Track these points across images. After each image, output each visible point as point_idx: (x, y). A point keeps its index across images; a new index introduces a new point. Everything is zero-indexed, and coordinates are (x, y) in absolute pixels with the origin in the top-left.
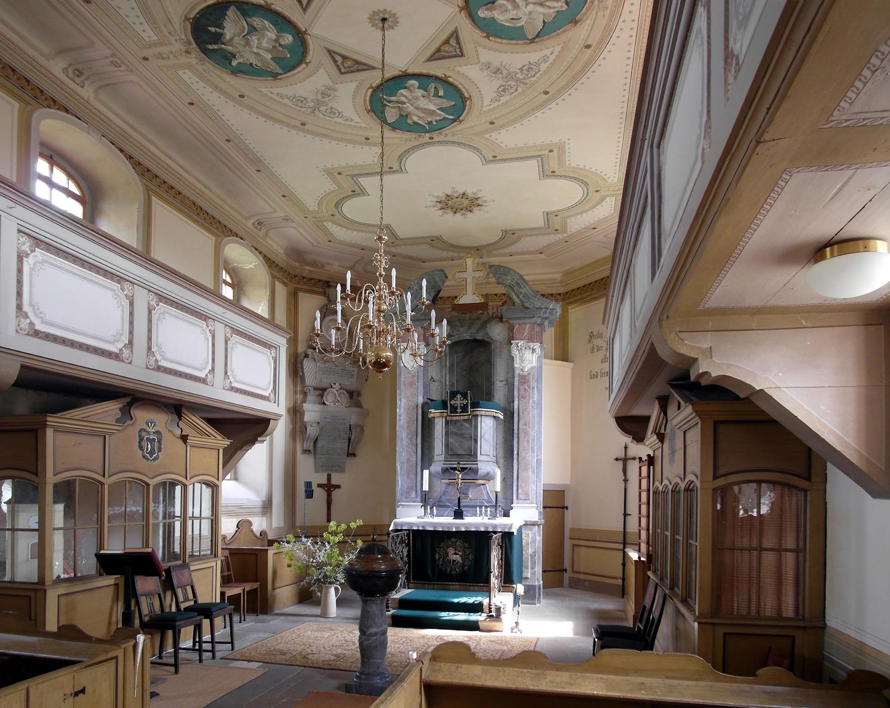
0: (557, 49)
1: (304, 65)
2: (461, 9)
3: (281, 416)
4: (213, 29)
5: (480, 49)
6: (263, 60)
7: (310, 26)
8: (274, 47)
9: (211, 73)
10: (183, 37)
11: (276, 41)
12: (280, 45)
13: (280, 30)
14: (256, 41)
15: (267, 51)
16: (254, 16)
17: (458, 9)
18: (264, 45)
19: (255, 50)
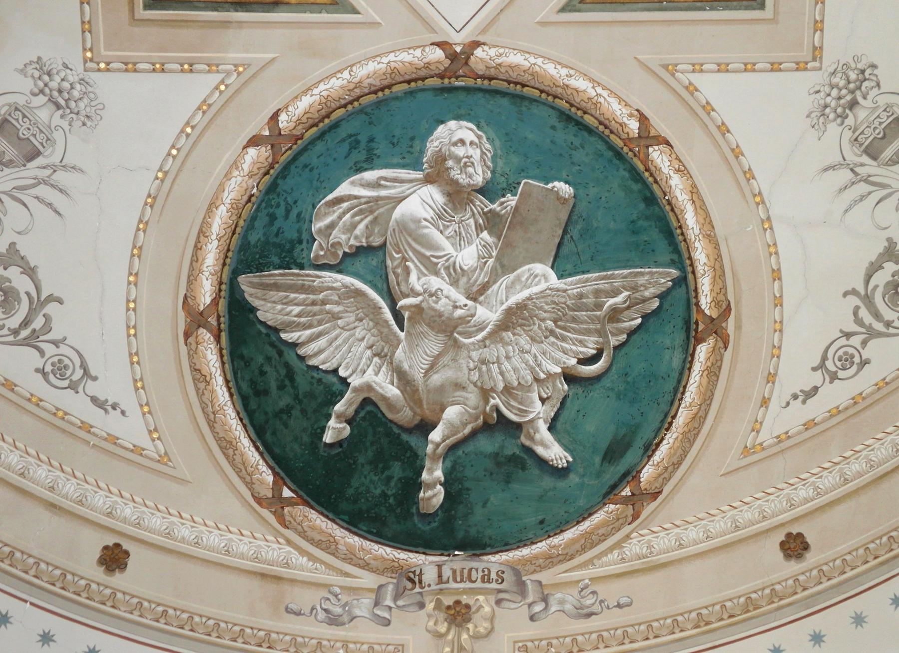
0: (131, 429)
1: (658, 156)
3: (339, 417)
4: (335, 430)
6: (565, 317)
7: (429, 26)
8: (492, 222)
9: (612, 592)
10: (369, 580)
11: (457, 196)
12: (487, 191)
13: (407, 151)
14: (435, 283)
15: (504, 266)
16: (305, 220)
18: (467, 257)
19: (488, 314)
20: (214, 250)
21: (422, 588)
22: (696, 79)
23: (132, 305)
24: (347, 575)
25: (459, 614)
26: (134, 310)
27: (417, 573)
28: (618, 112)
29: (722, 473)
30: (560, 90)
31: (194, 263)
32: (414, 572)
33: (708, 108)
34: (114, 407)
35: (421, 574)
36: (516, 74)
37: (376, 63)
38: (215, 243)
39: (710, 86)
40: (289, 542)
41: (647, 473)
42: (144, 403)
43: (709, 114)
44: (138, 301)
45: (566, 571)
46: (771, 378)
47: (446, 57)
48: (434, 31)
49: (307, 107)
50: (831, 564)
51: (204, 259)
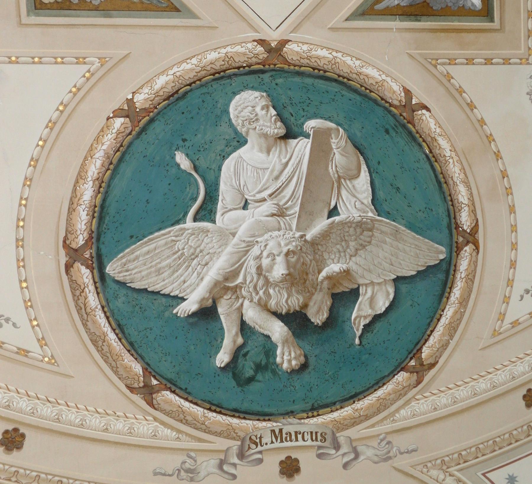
2: (276, 50)
5: (75, 74)
17: (273, 37)
20: (89, 188)
21: (262, 446)
22: (451, 69)
23: (24, 202)
24: (200, 440)
25: (290, 467)
26: (25, 206)
27: (259, 436)
28: (394, 91)
29: (480, 348)
30: (354, 76)
31: (73, 199)
32: (256, 436)
33: (461, 91)
34: (7, 320)
35: (261, 438)
36: (322, 63)
37: (217, 53)
38: (91, 183)
39: (461, 75)
40: (155, 419)
41: (426, 352)
42: (33, 318)
43: (461, 95)
44: (32, 299)
45: (368, 428)
46: (510, 283)
47: (265, 51)
48: (257, 31)
49: (164, 83)
50: (502, 437)
51: (82, 195)
